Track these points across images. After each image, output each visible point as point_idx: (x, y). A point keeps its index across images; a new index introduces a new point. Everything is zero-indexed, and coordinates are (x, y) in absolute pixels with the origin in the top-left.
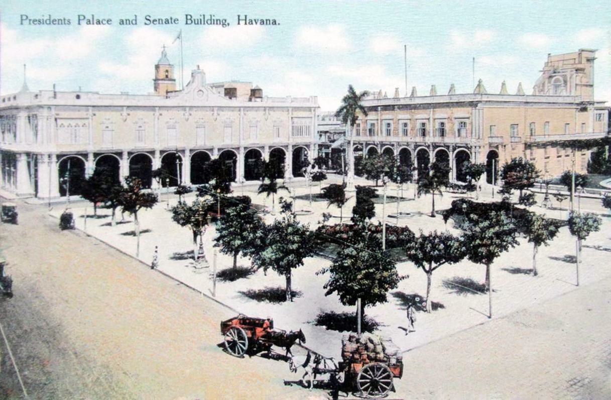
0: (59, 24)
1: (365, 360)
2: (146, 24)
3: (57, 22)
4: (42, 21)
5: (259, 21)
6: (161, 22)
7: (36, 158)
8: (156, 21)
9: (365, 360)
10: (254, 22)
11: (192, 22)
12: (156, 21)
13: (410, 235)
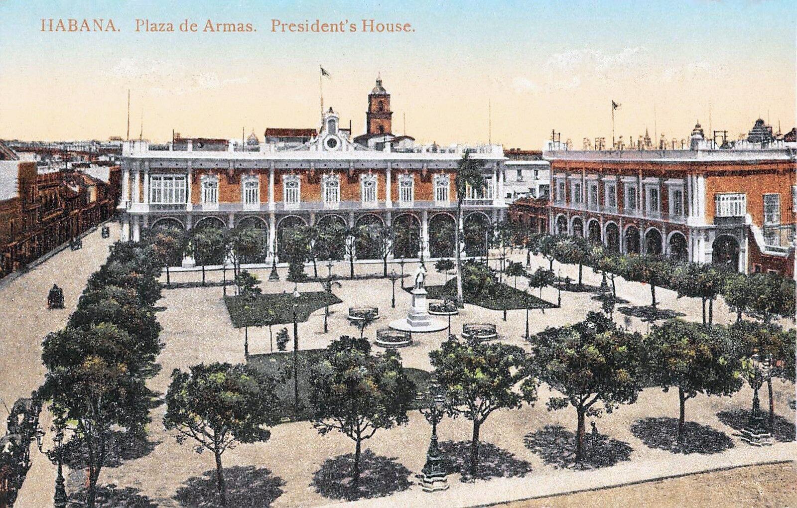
0: (332, 31)
1: (469, 345)
2: (351, 31)
3: (330, 28)
4: (305, 27)
5: (79, 26)
6: (390, 27)
7: (750, 230)
8: (328, 26)
9: (469, 345)
10: (67, 25)
11: (384, 28)
12: (328, 26)
13: (597, 264)
